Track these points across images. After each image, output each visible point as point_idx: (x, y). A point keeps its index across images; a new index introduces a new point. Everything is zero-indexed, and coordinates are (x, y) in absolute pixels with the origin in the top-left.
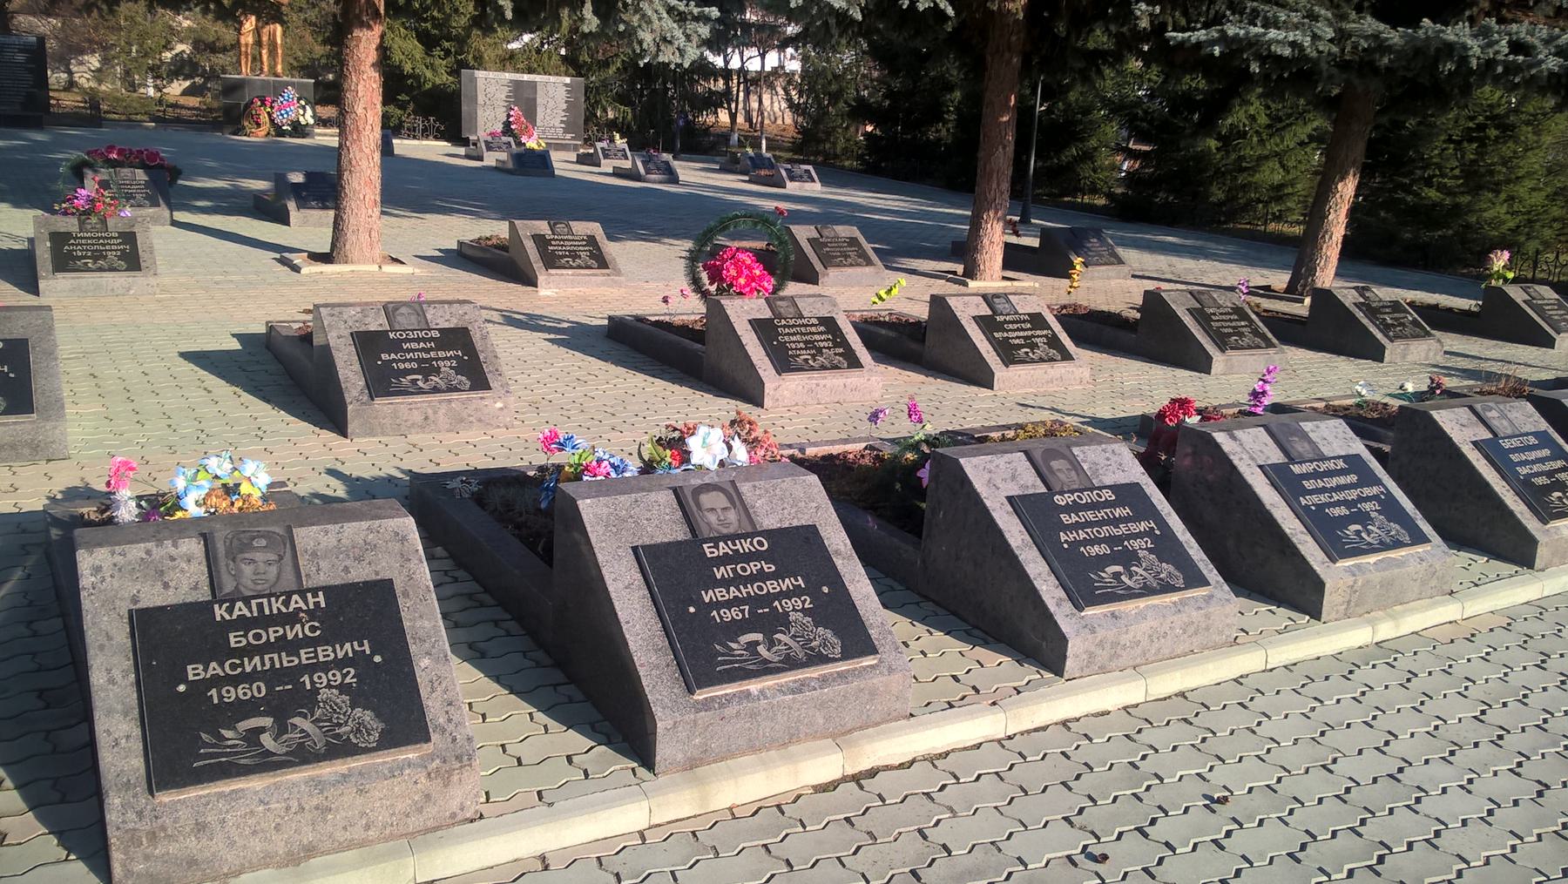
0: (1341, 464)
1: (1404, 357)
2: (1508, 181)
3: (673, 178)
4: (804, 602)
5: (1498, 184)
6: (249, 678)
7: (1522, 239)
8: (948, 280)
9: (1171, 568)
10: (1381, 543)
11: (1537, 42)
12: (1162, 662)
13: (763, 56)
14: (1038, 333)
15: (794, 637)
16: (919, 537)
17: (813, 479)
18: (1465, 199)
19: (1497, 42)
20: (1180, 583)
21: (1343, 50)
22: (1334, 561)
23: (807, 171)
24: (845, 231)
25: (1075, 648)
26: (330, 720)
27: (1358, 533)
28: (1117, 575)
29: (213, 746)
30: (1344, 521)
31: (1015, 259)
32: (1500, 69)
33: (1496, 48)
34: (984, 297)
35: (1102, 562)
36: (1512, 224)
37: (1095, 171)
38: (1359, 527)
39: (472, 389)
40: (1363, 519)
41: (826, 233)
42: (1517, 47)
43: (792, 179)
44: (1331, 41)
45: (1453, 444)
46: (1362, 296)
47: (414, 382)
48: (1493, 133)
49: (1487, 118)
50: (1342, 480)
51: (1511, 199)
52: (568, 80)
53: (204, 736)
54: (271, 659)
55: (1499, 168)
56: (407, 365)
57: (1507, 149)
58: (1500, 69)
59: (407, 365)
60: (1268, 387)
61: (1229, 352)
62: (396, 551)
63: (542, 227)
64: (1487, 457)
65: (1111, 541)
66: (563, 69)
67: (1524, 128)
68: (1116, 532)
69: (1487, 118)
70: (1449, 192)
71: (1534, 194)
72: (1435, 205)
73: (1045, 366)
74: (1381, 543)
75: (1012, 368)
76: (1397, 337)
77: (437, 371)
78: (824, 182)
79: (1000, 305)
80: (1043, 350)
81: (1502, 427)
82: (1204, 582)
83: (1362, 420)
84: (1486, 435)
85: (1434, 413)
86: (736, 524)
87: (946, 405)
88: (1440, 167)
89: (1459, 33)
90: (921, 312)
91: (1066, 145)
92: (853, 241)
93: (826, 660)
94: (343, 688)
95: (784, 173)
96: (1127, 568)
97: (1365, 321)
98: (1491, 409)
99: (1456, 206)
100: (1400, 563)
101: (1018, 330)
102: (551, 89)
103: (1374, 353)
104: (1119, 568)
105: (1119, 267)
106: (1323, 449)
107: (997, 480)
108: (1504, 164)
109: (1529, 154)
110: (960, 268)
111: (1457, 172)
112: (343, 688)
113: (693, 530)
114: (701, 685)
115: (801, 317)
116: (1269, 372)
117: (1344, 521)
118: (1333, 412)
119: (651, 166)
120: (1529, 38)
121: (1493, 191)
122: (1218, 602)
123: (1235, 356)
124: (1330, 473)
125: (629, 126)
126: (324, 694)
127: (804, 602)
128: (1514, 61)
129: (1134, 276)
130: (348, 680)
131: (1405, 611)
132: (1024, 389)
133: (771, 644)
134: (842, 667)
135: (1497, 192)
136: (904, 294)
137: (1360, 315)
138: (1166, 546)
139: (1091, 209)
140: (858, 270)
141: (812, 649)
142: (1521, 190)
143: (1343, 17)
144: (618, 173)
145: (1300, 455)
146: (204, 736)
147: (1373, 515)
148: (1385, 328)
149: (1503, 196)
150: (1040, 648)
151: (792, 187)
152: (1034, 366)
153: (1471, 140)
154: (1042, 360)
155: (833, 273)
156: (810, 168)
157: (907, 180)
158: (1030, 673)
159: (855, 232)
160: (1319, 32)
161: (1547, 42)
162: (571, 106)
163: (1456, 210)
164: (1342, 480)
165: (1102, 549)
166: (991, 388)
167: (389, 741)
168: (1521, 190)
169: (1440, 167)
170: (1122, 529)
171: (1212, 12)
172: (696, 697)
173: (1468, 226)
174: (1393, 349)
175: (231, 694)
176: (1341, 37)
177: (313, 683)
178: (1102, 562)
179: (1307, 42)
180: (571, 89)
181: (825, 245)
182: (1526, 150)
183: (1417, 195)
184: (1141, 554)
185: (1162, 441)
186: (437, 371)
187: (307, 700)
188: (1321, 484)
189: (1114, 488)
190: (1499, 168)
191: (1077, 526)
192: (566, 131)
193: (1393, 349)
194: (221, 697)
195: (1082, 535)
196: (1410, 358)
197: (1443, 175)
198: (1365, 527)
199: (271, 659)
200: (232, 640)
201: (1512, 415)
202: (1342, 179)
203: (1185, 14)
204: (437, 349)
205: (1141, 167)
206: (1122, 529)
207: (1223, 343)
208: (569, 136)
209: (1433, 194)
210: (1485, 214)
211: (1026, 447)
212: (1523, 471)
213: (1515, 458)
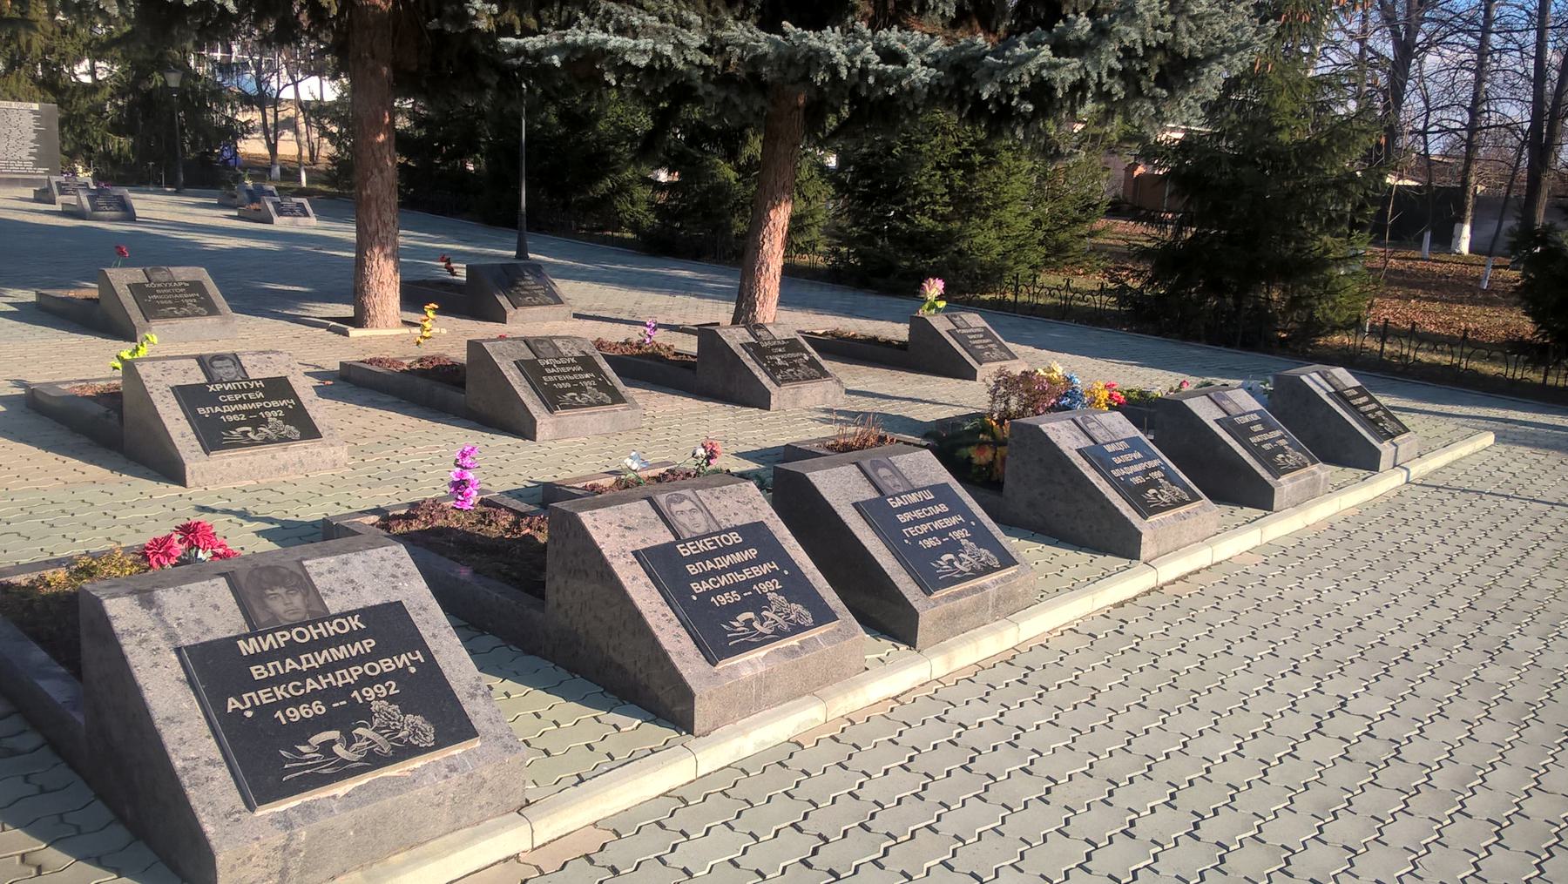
0: (355, 623)
1: (795, 403)
2: (995, 207)
3: (129, 215)
4: (388, 689)
5: (987, 209)
6: (308, 698)
7: (1010, 263)
8: (330, 329)
9: (799, 607)
10: (973, 570)
11: (907, 49)
12: (800, 706)
13: (295, 83)
14: (274, 403)
15: (376, 730)
16: (527, 596)
17: (402, 549)
18: (956, 225)
19: (862, 49)
20: (996, 564)
21: (726, 63)
22: (1145, 518)
23: (301, 205)
24: (183, 273)
25: (925, 622)
26: (388, 727)
27: (950, 562)
28: (748, 623)
29: (298, 761)
30: (936, 552)
31: (415, 295)
32: (871, 80)
33: (863, 54)
34: (200, 360)
35: (734, 609)
36: (1000, 249)
37: (633, 204)
38: (951, 556)
39: (302, 438)
40: (955, 547)
41: (157, 276)
42: (889, 55)
43: (280, 213)
44: (702, 48)
45: (603, 558)
46: (753, 335)
47: (245, 434)
48: (978, 158)
49: (971, 144)
50: (738, 558)
51: (999, 224)
52: (36, 106)
53: (283, 753)
54: (250, 698)
55: (986, 194)
56: (235, 417)
57: (992, 174)
58: (871, 80)
59: (235, 417)
60: (470, 475)
61: (560, 412)
62: (388, 576)
63: (137, 275)
64: (1093, 465)
65: (739, 587)
66: (37, 94)
67: (1004, 153)
68: (739, 578)
69: (971, 144)
70: (944, 219)
71: (1020, 219)
72: (929, 232)
73: (272, 448)
74: (973, 570)
75: (215, 455)
76: (786, 380)
77: (265, 422)
78: (322, 214)
79: (221, 369)
80: (591, 393)
81: (1099, 434)
82: (832, 617)
83: (948, 441)
84: (1088, 443)
85: (586, 518)
86: (704, 523)
87: (128, 509)
88: (931, 196)
89: (830, 41)
90: (460, 355)
91: (600, 177)
92: (196, 287)
93: (803, 629)
94: (391, 699)
95: (271, 207)
96: (758, 613)
97: (751, 364)
98: (682, 499)
99: (949, 232)
100: (399, 785)
101: (241, 401)
102: (14, 118)
103: (760, 400)
104: (751, 615)
105: (558, 308)
106: (914, 481)
107: (616, 535)
108: (990, 190)
109: (1012, 179)
110: (348, 311)
111: (947, 199)
112: (391, 699)
113: (879, 490)
114: (261, 802)
115: (246, 379)
116: (464, 455)
117: (936, 552)
118: (580, 496)
119: (100, 201)
120: (900, 45)
121: (980, 216)
122: (1207, 512)
123: (569, 417)
124: (337, 640)
125: (127, 158)
126: (376, 706)
127: (388, 689)
128: (884, 71)
129: (576, 316)
130: (392, 692)
131: (404, 865)
132: (236, 485)
133: (350, 741)
134: (438, 756)
135: (985, 217)
136: (446, 337)
137: (746, 358)
138: (796, 587)
139: (622, 243)
140: (197, 321)
141: (400, 740)
142: (1007, 215)
143: (720, 25)
144: (67, 213)
145: (275, 617)
146: (283, 753)
147: (964, 542)
148: (773, 370)
149: (990, 222)
150: (668, 706)
151: (281, 224)
152: (255, 450)
153: (957, 168)
154: (590, 404)
155: (157, 325)
156: (304, 201)
157: (442, 214)
158: (658, 733)
159: (202, 274)
160: (685, 41)
161: (921, 49)
162: (41, 137)
163: (949, 238)
164: (738, 558)
165: (734, 597)
166: (534, 439)
167: (818, 622)
168: (1007, 215)
169: (931, 196)
170: (746, 574)
171: (564, 13)
172: (719, 667)
173: (960, 253)
174: (780, 395)
175: (295, 714)
176: (714, 47)
177: (363, 698)
178: (734, 609)
179: (668, 50)
180: (40, 117)
181: (153, 291)
182: (1009, 175)
183: (910, 223)
184: (771, 596)
185: (784, 479)
186: (265, 422)
187: (363, 713)
188: (710, 566)
189: (740, 529)
190: (986, 194)
191: (704, 576)
192: (37, 164)
193: (780, 395)
194: (287, 718)
195: (280, 693)
196: (803, 403)
197: (935, 203)
198: (956, 555)
199: (250, 698)
200: (255, 674)
201: (713, 506)
202: (773, 206)
203: (537, 17)
204: (268, 398)
205: (668, 200)
206: (746, 574)
207: (552, 400)
208: (41, 170)
209: (926, 222)
210: (976, 240)
211: (647, 494)
212: (698, 588)
213: (904, 518)
